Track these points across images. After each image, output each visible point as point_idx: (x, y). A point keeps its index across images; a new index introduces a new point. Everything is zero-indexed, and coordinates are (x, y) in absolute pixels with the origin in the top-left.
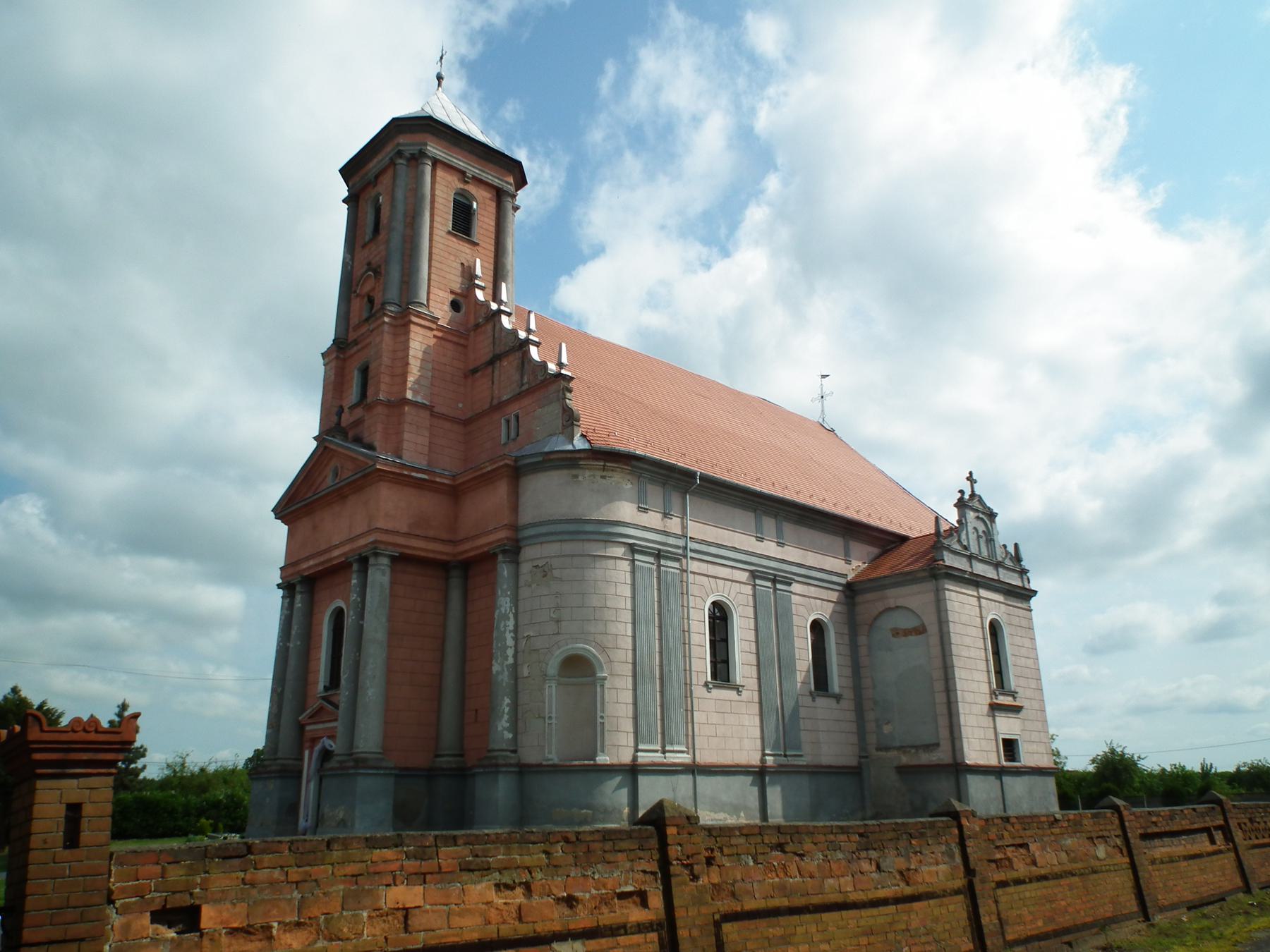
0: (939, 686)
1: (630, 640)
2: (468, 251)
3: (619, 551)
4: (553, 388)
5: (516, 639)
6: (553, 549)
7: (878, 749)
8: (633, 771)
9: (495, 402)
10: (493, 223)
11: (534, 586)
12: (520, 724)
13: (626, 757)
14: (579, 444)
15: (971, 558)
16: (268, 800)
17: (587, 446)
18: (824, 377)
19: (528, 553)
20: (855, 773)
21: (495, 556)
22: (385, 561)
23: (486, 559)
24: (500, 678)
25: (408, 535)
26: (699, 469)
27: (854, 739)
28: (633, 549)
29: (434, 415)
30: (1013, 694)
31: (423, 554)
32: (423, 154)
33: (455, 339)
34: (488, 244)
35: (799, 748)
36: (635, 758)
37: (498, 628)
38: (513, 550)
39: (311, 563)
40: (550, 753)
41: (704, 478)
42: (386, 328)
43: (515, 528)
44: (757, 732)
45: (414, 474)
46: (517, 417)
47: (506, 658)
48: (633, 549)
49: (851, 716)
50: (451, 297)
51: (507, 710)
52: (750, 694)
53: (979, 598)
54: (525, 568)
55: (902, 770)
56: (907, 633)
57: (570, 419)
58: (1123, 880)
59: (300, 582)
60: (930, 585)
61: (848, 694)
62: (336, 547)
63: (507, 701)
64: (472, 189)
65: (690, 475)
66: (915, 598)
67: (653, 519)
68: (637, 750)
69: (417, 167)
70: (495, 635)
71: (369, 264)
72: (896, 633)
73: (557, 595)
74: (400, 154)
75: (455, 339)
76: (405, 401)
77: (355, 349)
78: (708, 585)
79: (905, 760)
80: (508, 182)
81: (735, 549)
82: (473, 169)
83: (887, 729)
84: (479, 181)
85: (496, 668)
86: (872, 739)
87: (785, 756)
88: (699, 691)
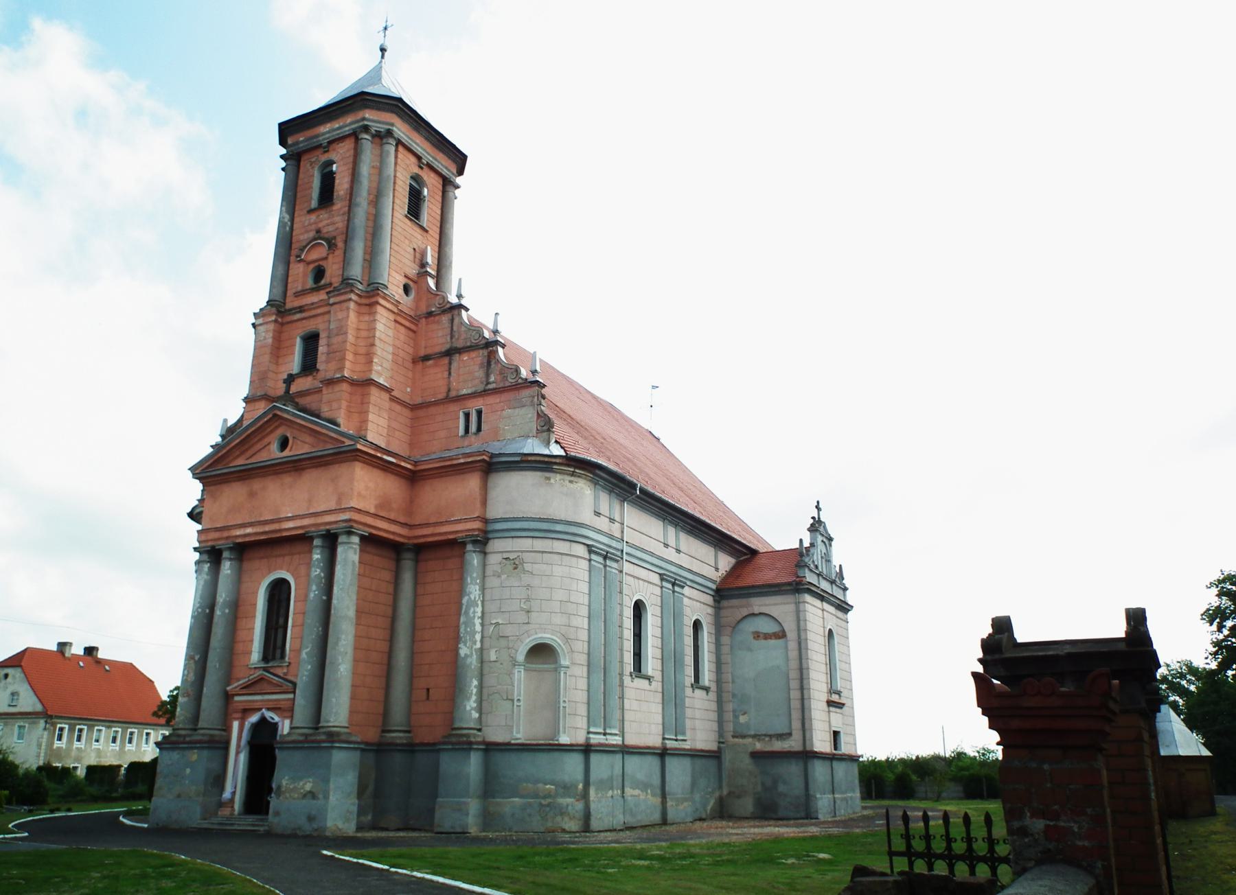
0: (794, 684)
1: (586, 632)
2: (419, 237)
3: (581, 551)
4: (526, 393)
5: (482, 625)
6: (526, 544)
7: (734, 737)
10: (439, 212)
11: (504, 577)
12: (484, 704)
13: (580, 738)
14: (556, 450)
16: (188, 771)
17: (562, 453)
18: (654, 387)
19: (496, 545)
20: (714, 756)
21: (464, 544)
22: (356, 539)
23: (453, 547)
24: (469, 660)
25: (375, 516)
27: (715, 726)
29: (394, 399)
30: (839, 693)
31: (385, 535)
33: (407, 324)
35: (684, 733)
36: (588, 739)
37: (467, 613)
38: (482, 541)
39: (249, 530)
40: (518, 732)
42: (352, 305)
44: (659, 719)
45: (385, 457)
46: (479, 413)
47: (475, 643)
49: (714, 706)
50: (404, 281)
51: (475, 691)
52: (657, 685)
53: (674, 592)
54: (493, 559)
55: (756, 755)
56: (767, 636)
59: (230, 549)
60: (790, 598)
61: (713, 687)
62: (288, 519)
63: (475, 683)
66: (779, 607)
68: (589, 733)
69: (382, 145)
70: (462, 619)
71: (318, 231)
72: (757, 635)
73: (528, 587)
74: (366, 129)
75: (407, 324)
76: (370, 382)
77: (298, 316)
78: (640, 585)
79: (759, 746)
80: (444, 164)
81: (643, 550)
83: (742, 719)
85: (463, 651)
86: (729, 727)
87: (605, 734)
88: (627, 680)
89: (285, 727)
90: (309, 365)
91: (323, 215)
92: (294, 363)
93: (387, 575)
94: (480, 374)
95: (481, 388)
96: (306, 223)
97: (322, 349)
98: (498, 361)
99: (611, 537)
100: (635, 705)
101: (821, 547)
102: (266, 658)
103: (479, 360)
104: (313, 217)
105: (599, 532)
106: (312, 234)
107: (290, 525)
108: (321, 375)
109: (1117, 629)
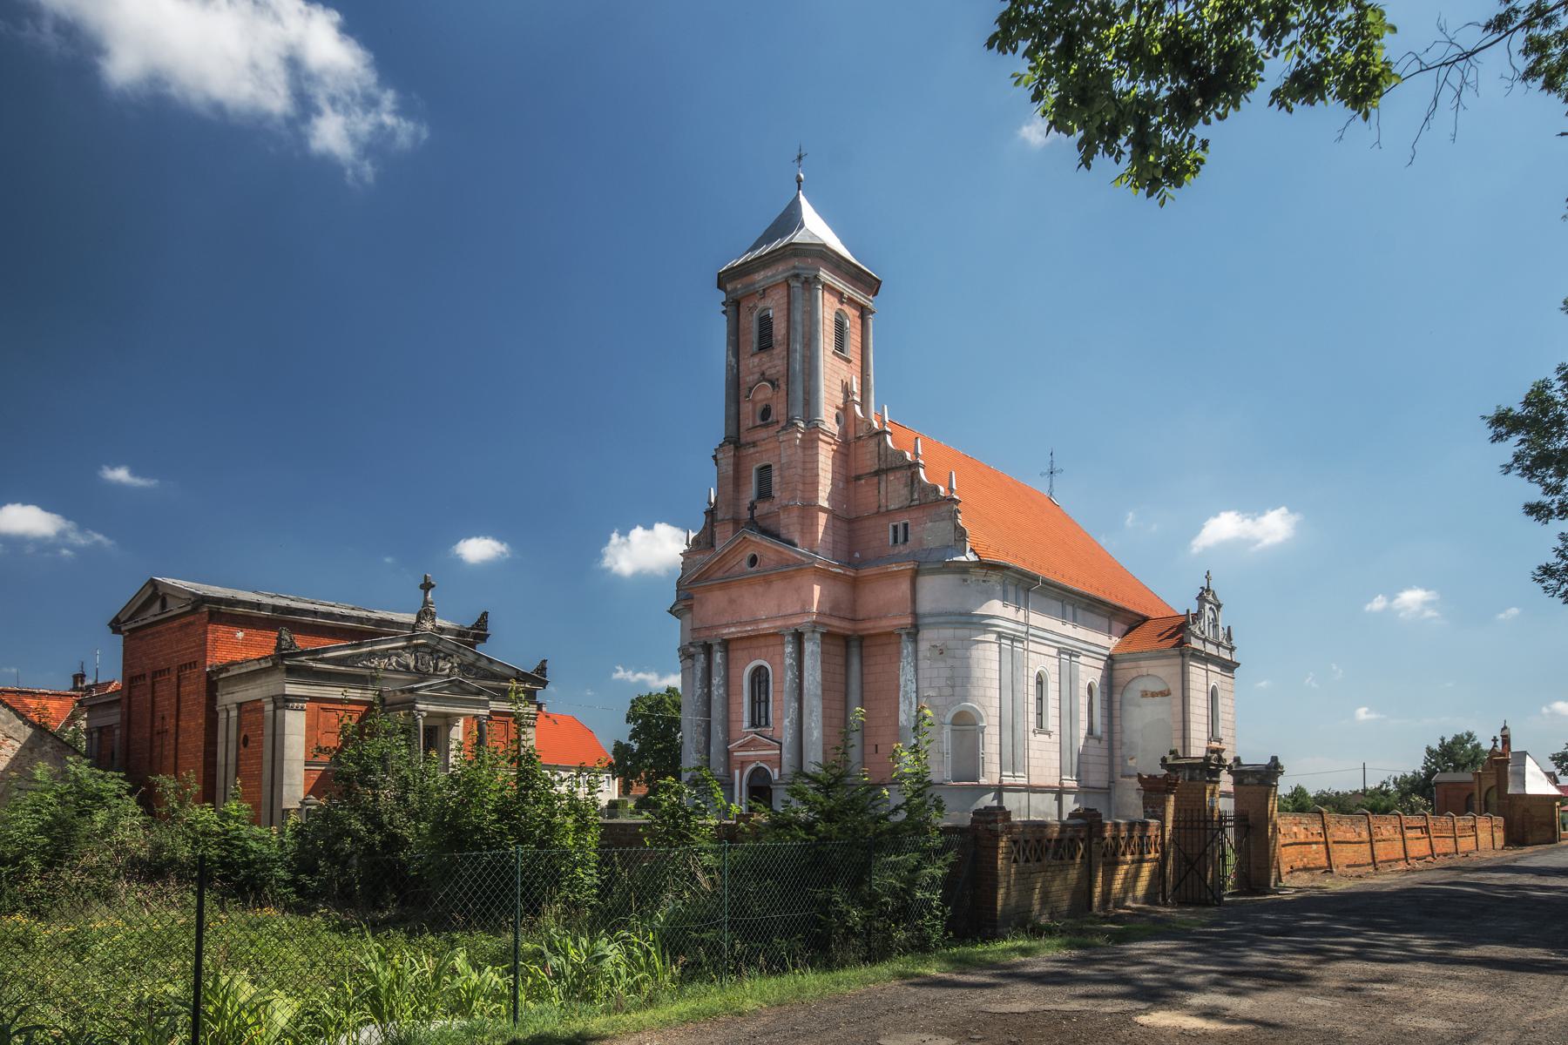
3: (993, 637)
4: (944, 508)
8: (1000, 790)
9: (883, 509)
14: (972, 558)
15: (1205, 640)
26: (1043, 573)
28: (1000, 636)
30: (1220, 741)
32: (816, 278)
34: (856, 360)
38: (914, 633)
41: (1046, 582)
43: (915, 614)
48: (1000, 636)
49: (1105, 753)
52: (1055, 738)
54: (924, 646)
56: (1154, 695)
57: (961, 534)
58: (1400, 844)
61: (1105, 736)
64: (846, 308)
65: (1035, 578)
67: (1010, 612)
71: (763, 374)
72: (1145, 694)
82: (848, 291)
84: (851, 301)
86: (1118, 770)
89: (775, 774)
90: (765, 493)
91: (765, 356)
92: (751, 492)
93: (840, 660)
94: (905, 492)
95: (907, 503)
96: (752, 364)
97: (775, 479)
98: (920, 480)
99: (1018, 623)
100: (1038, 754)
101: (1209, 614)
102: (753, 724)
103: (903, 481)
104: (756, 360)
105: (1008, 620)
106: (756, 376)
107: (766, 625)
108: (777, 501)
109: (1267, 761)
